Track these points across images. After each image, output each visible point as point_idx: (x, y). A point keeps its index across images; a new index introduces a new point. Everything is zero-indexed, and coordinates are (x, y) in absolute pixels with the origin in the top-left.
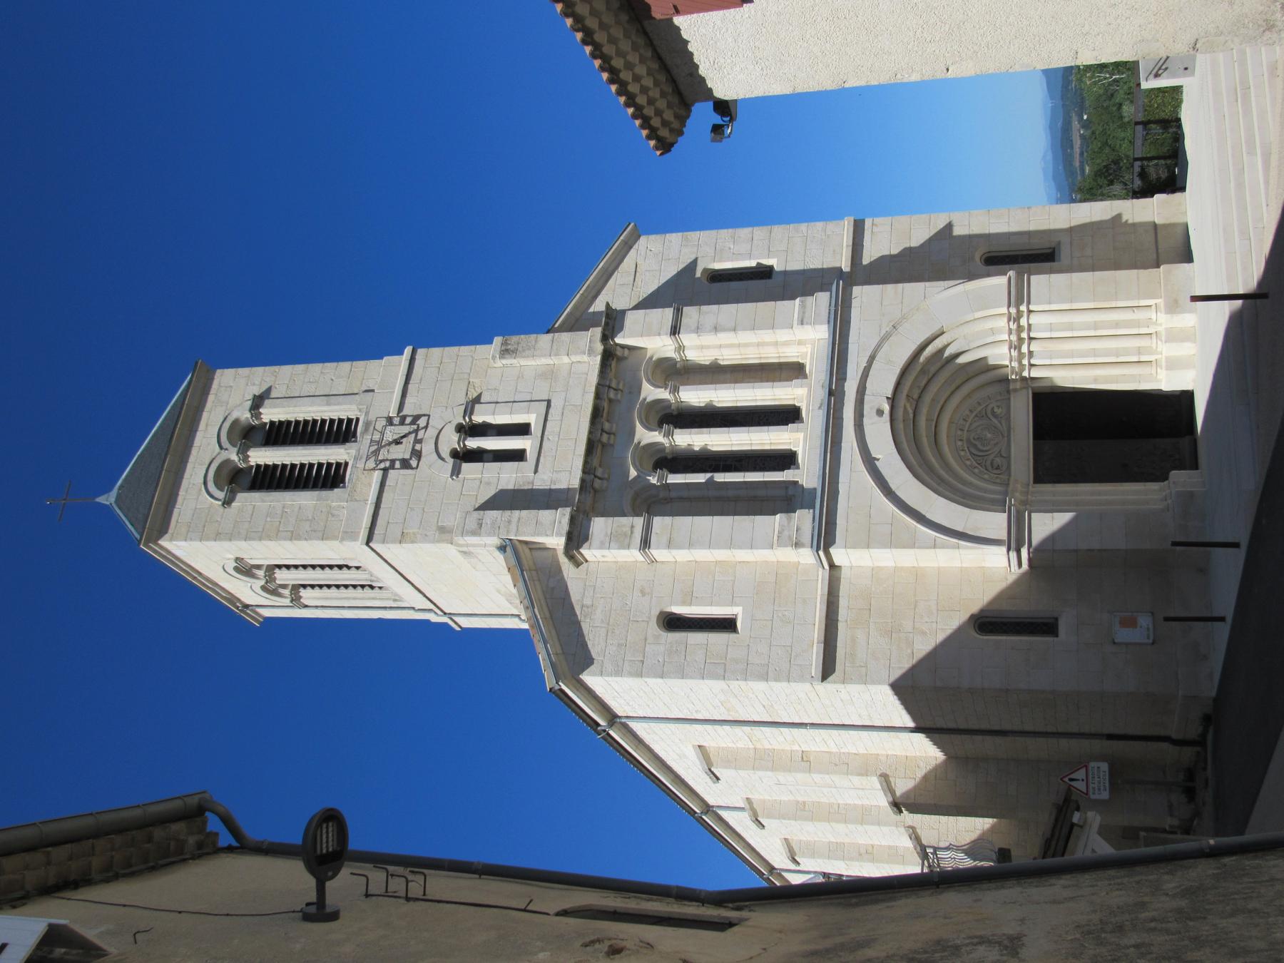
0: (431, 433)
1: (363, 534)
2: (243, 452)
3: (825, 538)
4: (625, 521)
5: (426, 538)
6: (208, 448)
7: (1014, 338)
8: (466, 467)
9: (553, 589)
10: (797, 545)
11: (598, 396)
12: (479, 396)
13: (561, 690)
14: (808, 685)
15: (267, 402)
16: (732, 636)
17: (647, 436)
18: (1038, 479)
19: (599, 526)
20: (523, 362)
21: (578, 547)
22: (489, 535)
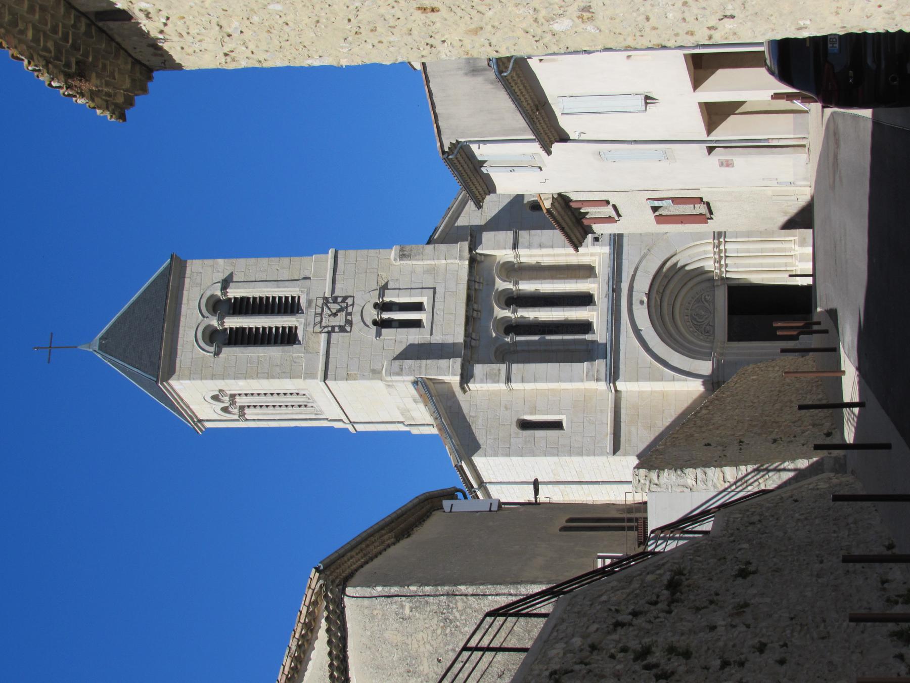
0: (357, 309)
1: (320, 374)
2: (221, 319)
3: (613, 376)
4: (495, 366)
5: (363, 377)
6: (192, 318)
7: (717, 256)
8: (384, 331)
9: (450, 407)
10: (598, 380)
11: (469, 288)
12: (387, 283)
13: (461, 466)
14: (605, 458)
15: (231, 284)
16: (561, 431)
17: (501, 313)
18: (730, 339)
19: (479, 369)
20: (414, 262)
21: (467, 382)
22: (408, 375)
